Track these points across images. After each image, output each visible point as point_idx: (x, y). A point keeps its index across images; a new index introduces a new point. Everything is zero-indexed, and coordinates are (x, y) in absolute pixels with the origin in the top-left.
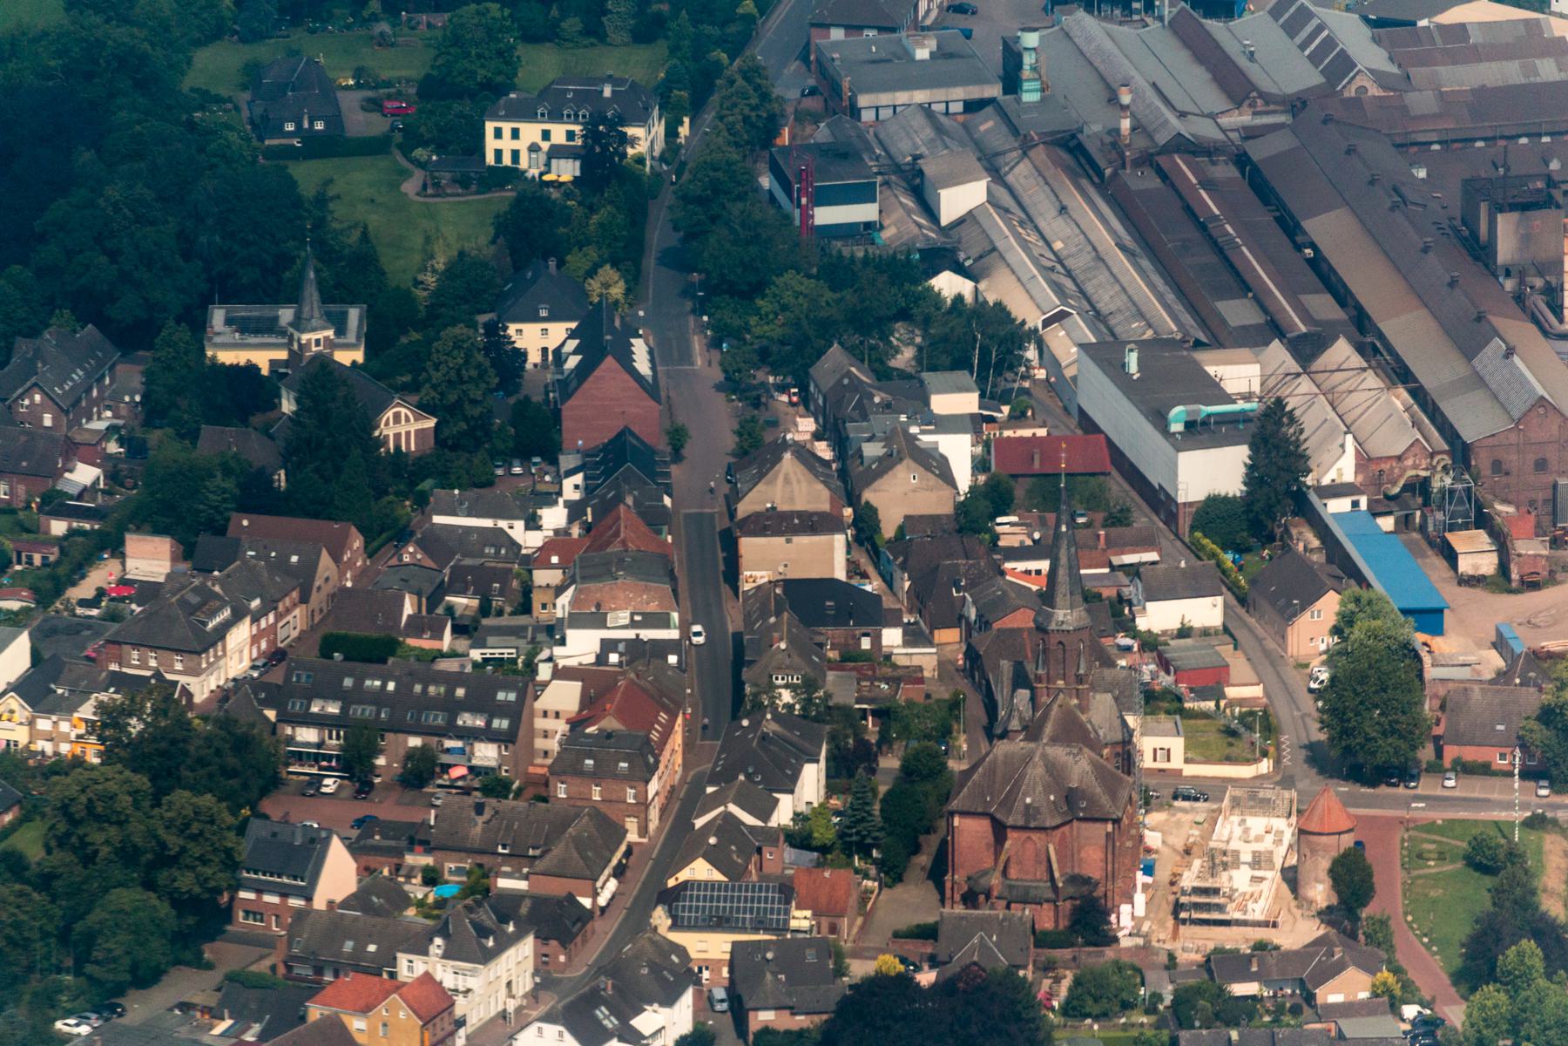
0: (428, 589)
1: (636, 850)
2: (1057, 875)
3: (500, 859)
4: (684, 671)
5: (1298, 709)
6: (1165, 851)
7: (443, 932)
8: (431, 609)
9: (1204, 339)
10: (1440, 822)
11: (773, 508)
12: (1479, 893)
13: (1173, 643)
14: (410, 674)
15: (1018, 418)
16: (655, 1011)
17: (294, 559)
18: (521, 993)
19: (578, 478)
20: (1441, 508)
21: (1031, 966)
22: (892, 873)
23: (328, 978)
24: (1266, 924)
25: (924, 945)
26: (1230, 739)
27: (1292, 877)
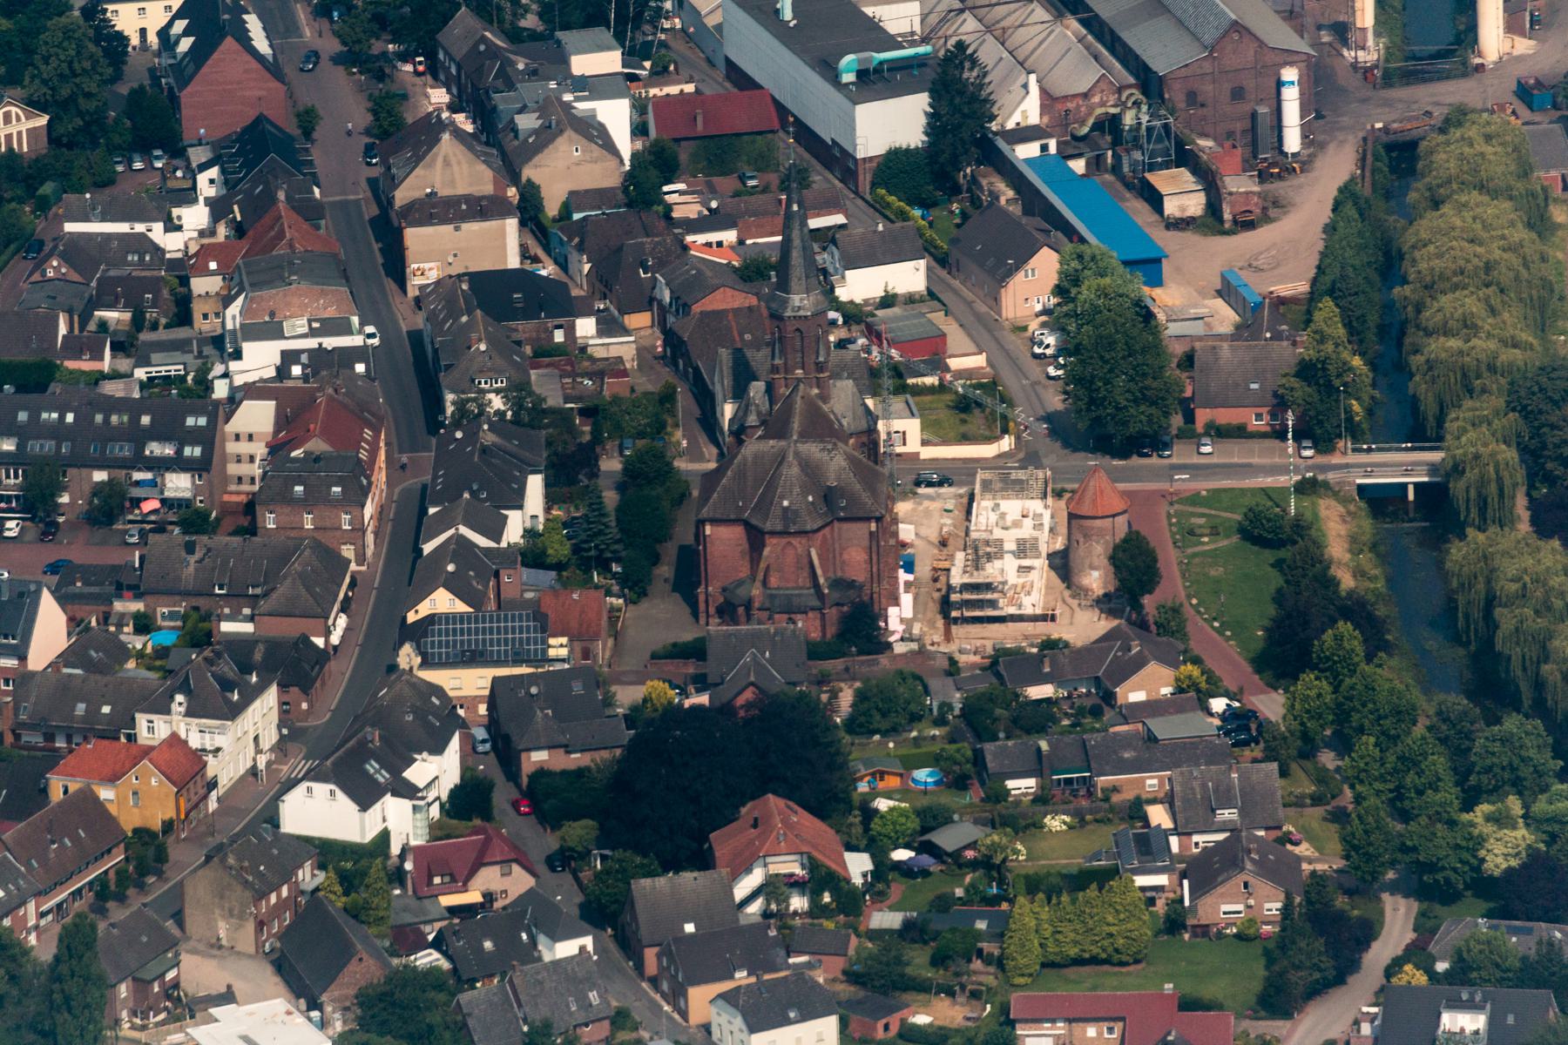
0: (79, 305)
1: (359, 578)
2: (822, 581)
4: (373, 380)
5: (1027, 378)
6: (918, 542)
7: (185, 688)
10: (1204, 493)
11: (433, 194)
12: (1261, 565)
13: (880, 313)
14: (90, 404)
15: (661, 74)
16: (424, 760)
22: (635, 586)
23: (60, 744)
25: (685, 664)
26: (963, 416)
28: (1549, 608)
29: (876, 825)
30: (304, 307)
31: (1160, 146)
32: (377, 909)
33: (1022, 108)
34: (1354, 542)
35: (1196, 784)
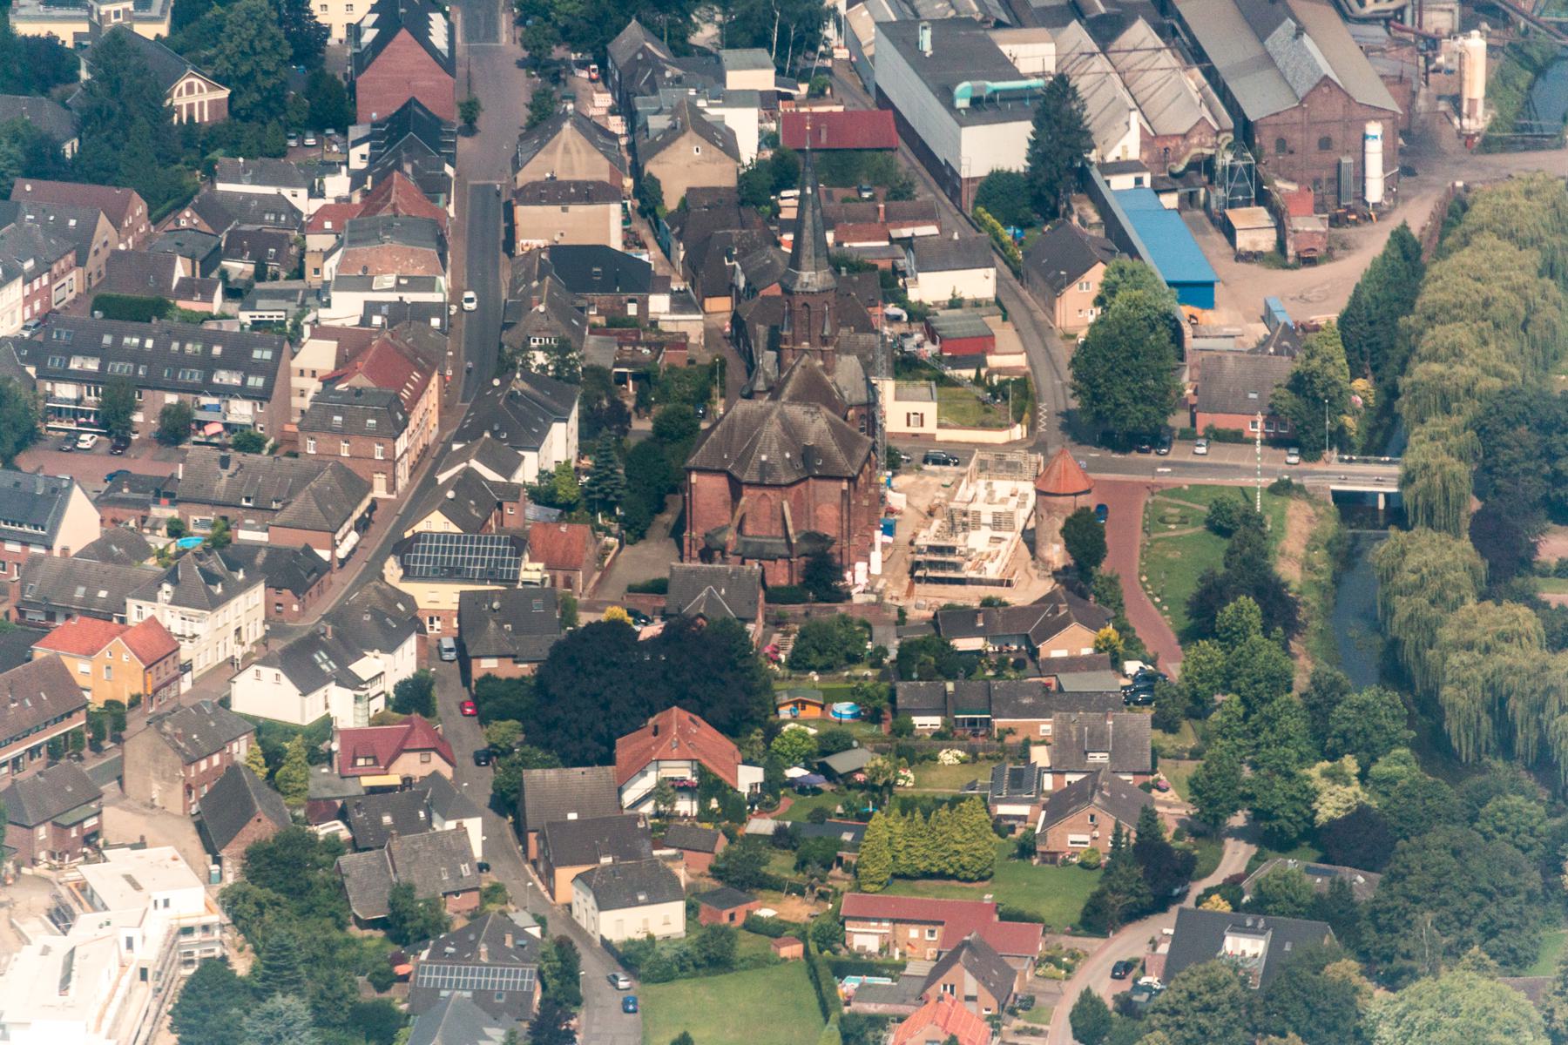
0: (202, 253)
2: (791, 531)
3: (240, 512)
7: (172, 577)
8: (205, 273)
9: (1004, 17)
13: (941, 313)
15: (816, 95)
17: (72, 223)
18: (252, 640)
19: (365, 148)
20: (1222, 184)
21: (760, 618)
24: (1000, 583)
27: (1030, 539)
28: (1444, 600)
29: (776, 743)
30: (394, 265)
31: (1241, 185)
32: (294, 781)
33: (1122, 142)
34: (1312, 543)
35: (1073, 729)
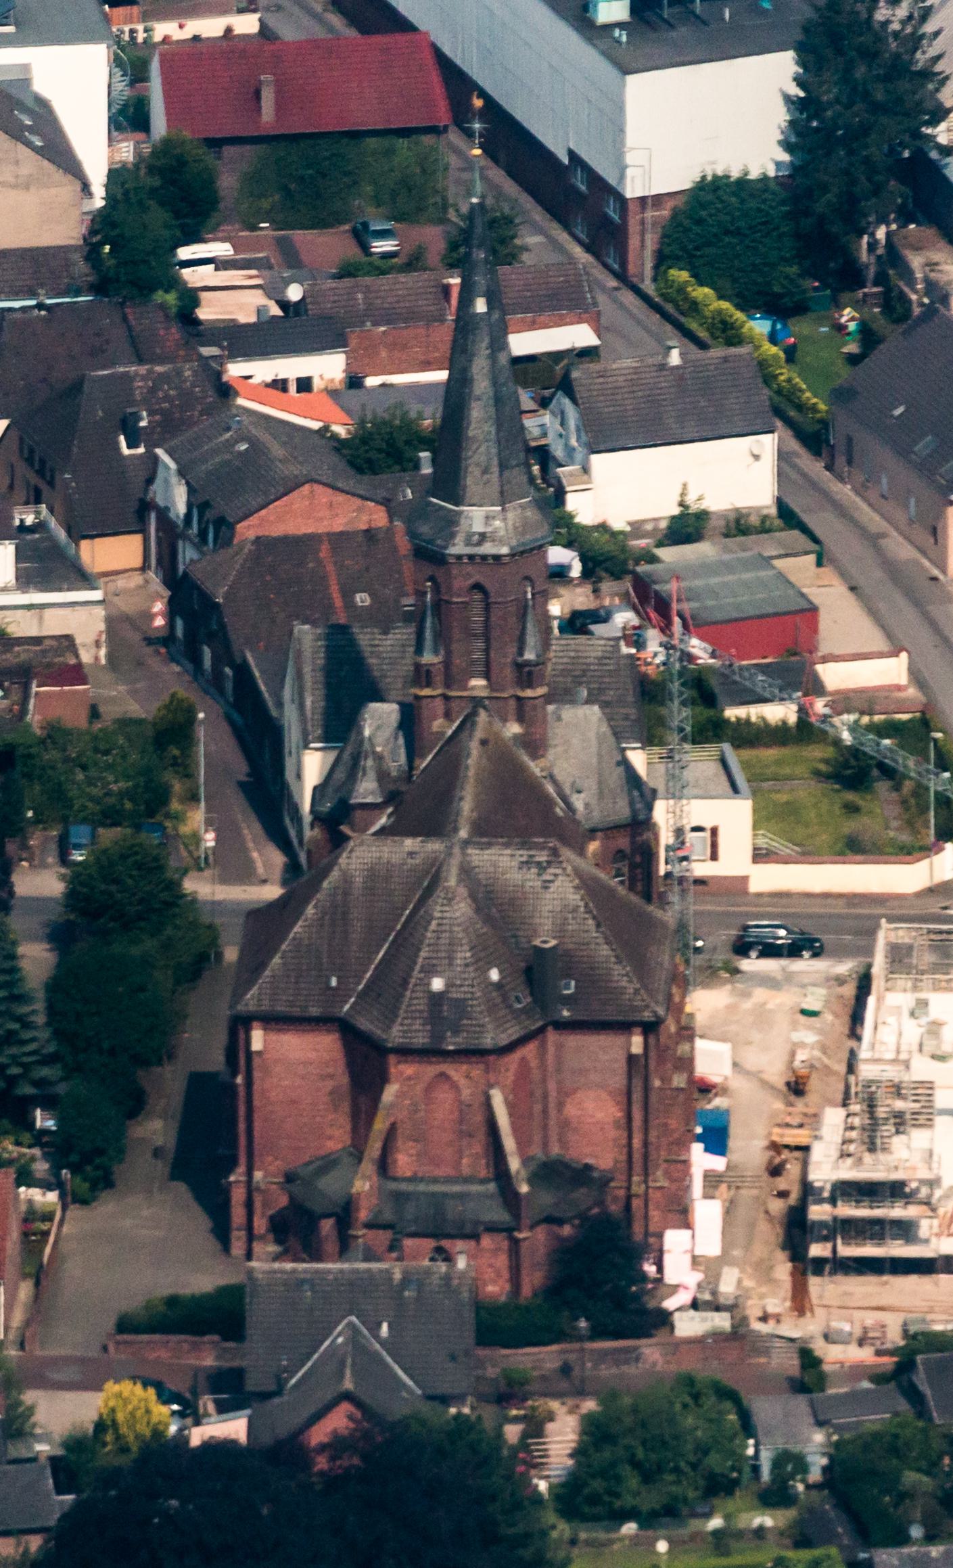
2: (514, 1164)
6: (738, 1084)
13: (669, 554)
25: (195, 1347)
26: (850, 796)
